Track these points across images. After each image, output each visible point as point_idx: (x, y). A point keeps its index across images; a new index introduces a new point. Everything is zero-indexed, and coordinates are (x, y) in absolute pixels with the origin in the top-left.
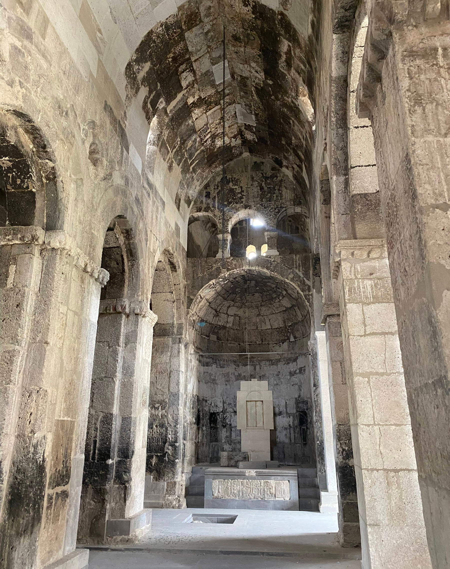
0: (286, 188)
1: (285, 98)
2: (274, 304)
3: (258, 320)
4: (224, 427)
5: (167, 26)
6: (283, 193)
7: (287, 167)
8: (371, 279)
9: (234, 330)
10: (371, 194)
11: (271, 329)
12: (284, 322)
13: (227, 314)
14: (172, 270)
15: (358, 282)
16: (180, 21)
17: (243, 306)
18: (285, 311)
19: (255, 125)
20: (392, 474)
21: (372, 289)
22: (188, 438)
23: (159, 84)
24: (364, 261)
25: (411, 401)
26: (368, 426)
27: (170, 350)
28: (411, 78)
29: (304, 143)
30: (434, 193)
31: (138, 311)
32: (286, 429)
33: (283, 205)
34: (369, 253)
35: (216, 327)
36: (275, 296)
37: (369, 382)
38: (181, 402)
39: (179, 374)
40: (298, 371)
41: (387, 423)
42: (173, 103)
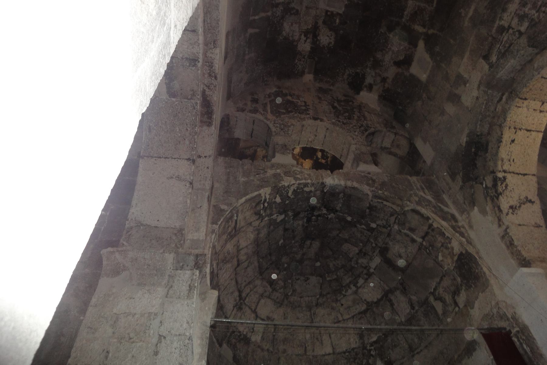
2: (343, 301)
3: (308, 336)
9: (263, 350)
11: (334, 353)
13: (255, 312)
14: (201, 121)
17: (286, 302)
18: (365, 312)
27: (165, 282)
35: (234, 332)
36: (347, 280)
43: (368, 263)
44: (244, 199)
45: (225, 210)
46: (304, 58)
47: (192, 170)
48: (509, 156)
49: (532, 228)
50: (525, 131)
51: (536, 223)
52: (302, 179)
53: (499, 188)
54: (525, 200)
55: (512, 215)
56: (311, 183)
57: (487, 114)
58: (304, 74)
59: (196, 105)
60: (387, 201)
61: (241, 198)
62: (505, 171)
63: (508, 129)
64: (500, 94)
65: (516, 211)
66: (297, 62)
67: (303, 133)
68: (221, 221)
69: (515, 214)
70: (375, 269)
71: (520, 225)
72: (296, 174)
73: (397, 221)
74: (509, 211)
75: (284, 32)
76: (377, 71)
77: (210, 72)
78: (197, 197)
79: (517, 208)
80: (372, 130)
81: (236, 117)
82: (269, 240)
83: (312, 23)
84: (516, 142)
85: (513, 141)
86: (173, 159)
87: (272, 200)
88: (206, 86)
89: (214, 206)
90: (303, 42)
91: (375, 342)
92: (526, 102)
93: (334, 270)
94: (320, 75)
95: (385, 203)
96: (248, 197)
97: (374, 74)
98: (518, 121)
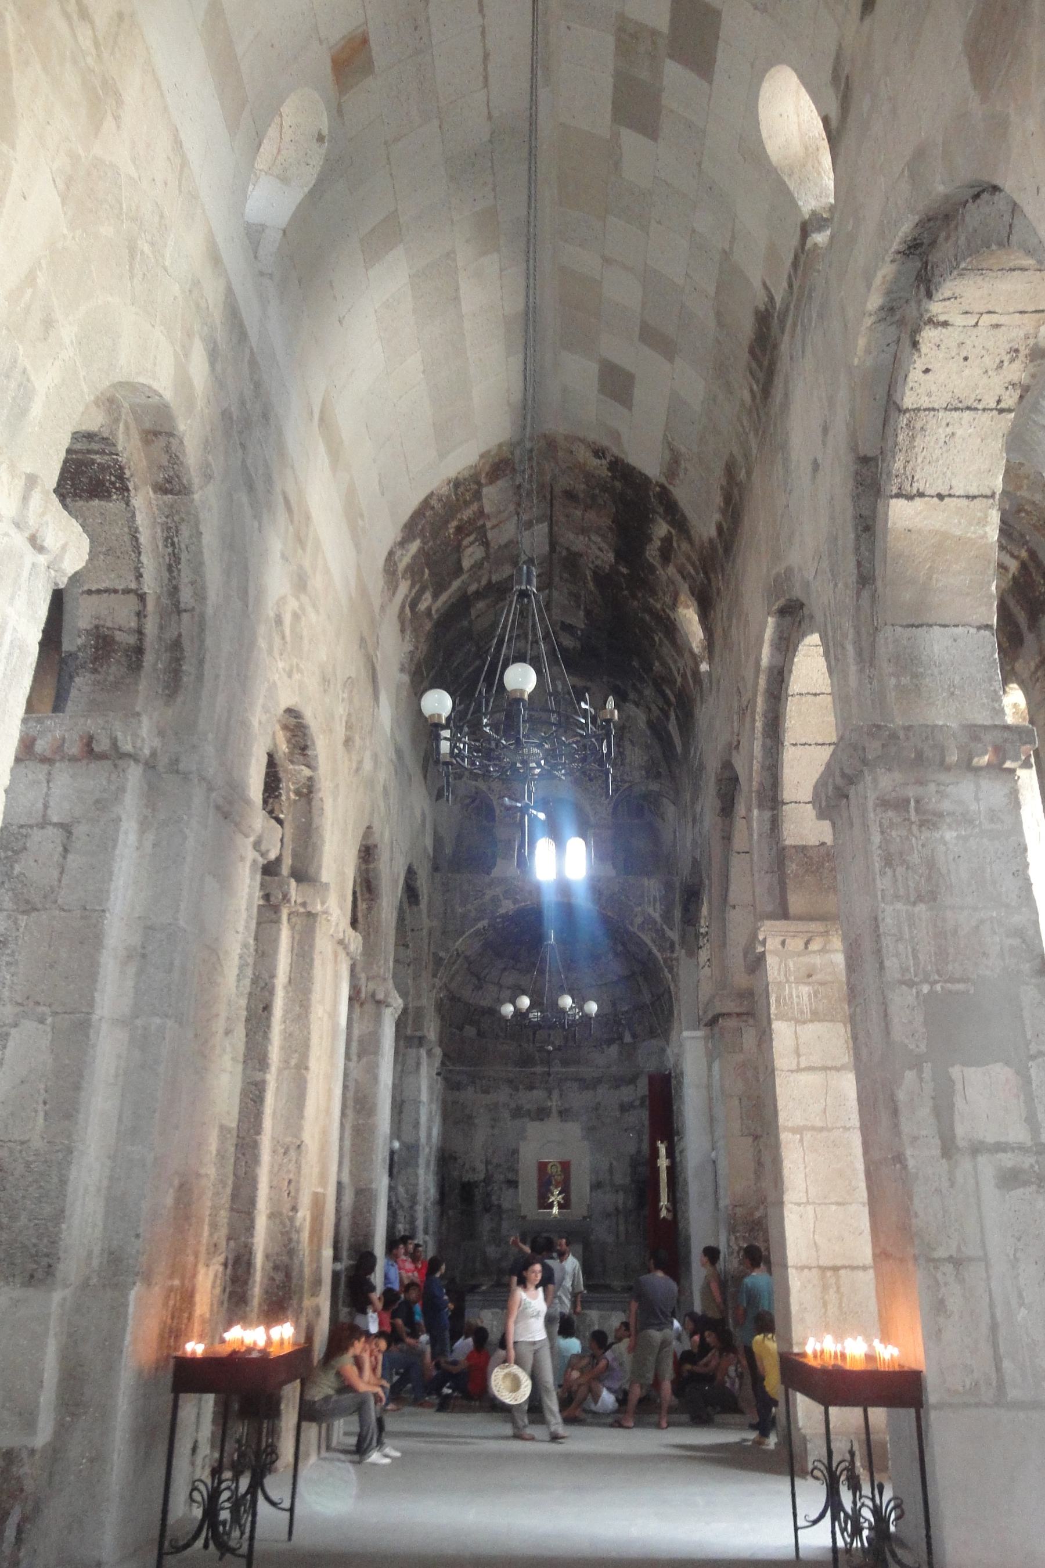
0: (632, 741)
1: (651, 600)
4: (487, 1210)
5: (457, 484)
6: (627, 753)
7: (637, 705)
8: (809, 984)
10: (812, 847)
12: (614, 1004)
15: (790, 987)
16: (480, 473)
19: (583, 626)
20: (829, 1274)
21: (810, 1000)
22: (431, 1232)
23: (427, 571)
24: (799, 955)
25: (869, 1175)
26: (799, 1204)
28: (882, 832)
29: (679, 680)
30: (901, 968)
31: (380, 996)
32: (609, 1215)
33: (625, 777)
34: (807, 944)
37: (801, 1140)
38: (422, 1161)
39: (419, 1107)
40: (637, 1103)
41: (827, 1201)
42: (444, 597)
91: (627, 1012)
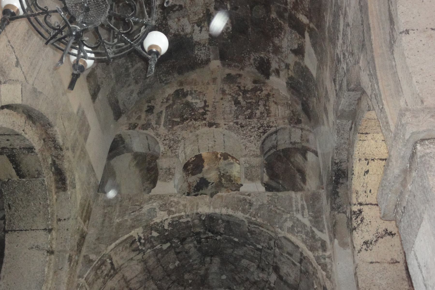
14: (57, 188)
43: (268, 278)
44: (113, 245)
45: (93, 260)
46: (204, 46)
47: (49, 239)
48: (365, 187)
49: (386, 265)
50: (379, 160)
51: (392, 259)
52: (176, 213)
53: (353, 222)
54: (384, 233)
55: (366, 251)
56: (185, 215)
57: (343, 141)
58: (210, 61)
59: (44, 182)
60: (262, 227)
61: (111, 244)
62: (361, 204)
63: (358, 161)
64: (350, 122)
65: (371, 246)
66: (198, 53)
67: (200, 141)
68: (87, 273)
69: (369, 250)
70: (274, 284)
71: (372, 263)
72: (172, 206)
73: (276, 245)
74: (362, 248)
75: (171, 30)
76: (279, 57)
77: (55, 146)
78: (59, 259)
79: (373, 243)
80: (273, 129)
81: (129, 135)
82: (161, 265)
83: (203, 11)
84: (370, 172)
85: (367, 172)
86: (32, 231)
87: (148, 236)
88: (55, 157)
89: (84, 256)
90: (199, 32)
92: (369, 137)
93: (240, 282)
94: (227, 60)
95: (261, 228)
96: (118, 242)
97: (277, 60)
98: (367, 152)
